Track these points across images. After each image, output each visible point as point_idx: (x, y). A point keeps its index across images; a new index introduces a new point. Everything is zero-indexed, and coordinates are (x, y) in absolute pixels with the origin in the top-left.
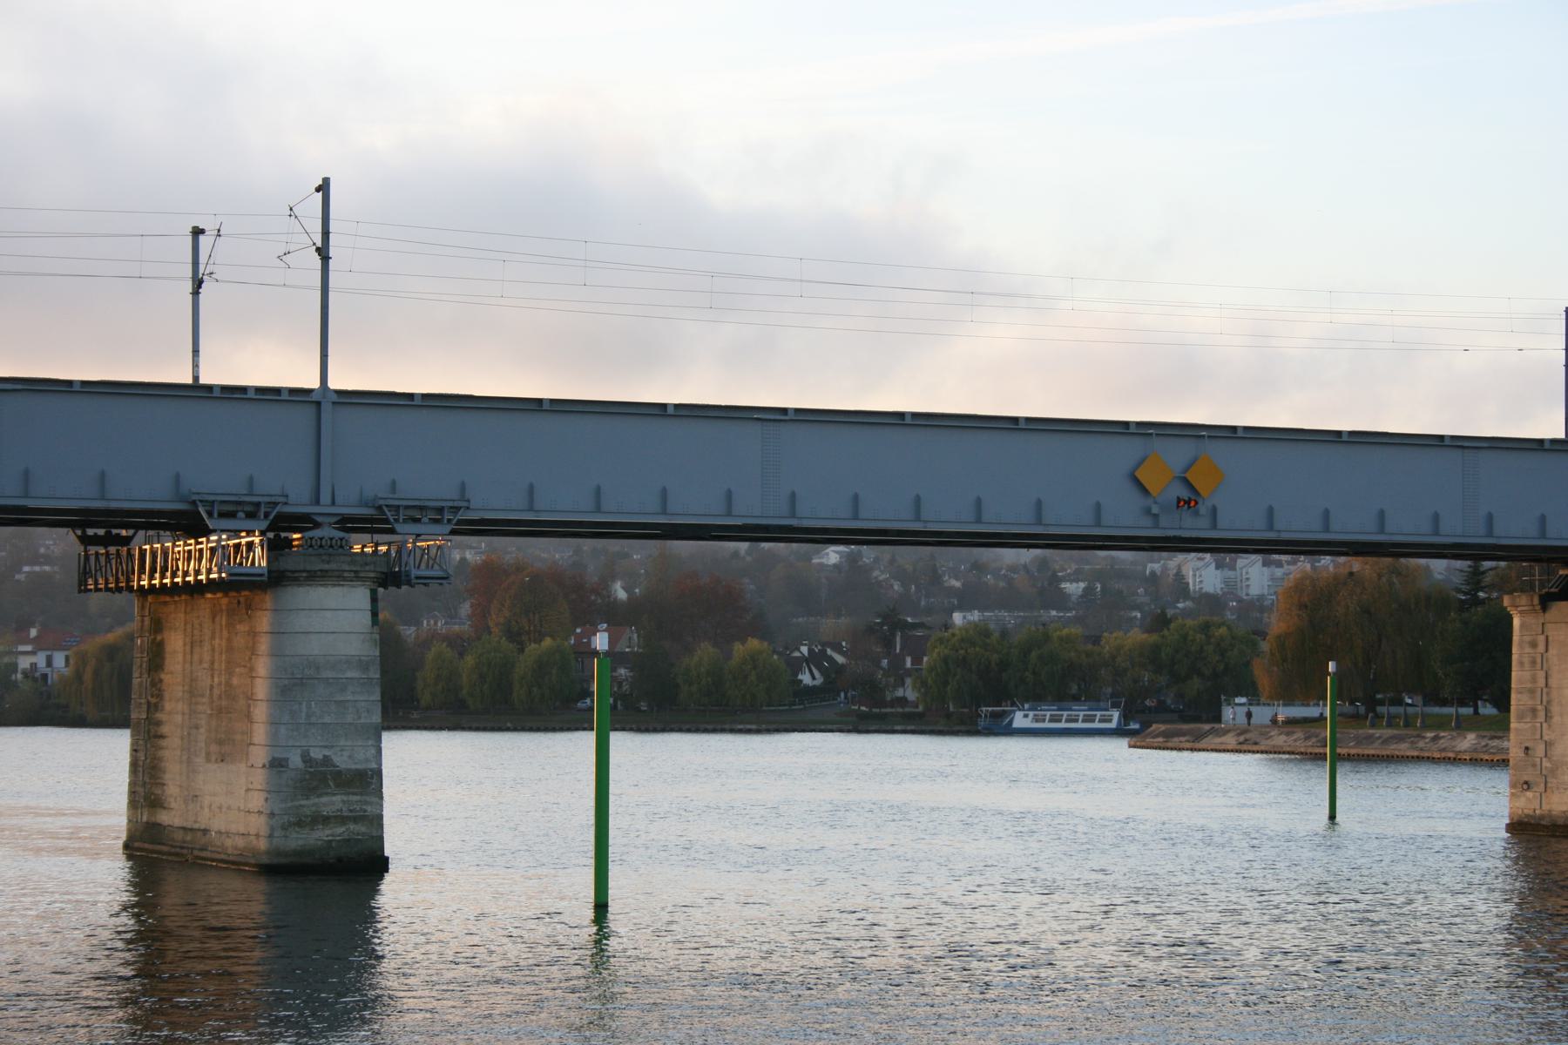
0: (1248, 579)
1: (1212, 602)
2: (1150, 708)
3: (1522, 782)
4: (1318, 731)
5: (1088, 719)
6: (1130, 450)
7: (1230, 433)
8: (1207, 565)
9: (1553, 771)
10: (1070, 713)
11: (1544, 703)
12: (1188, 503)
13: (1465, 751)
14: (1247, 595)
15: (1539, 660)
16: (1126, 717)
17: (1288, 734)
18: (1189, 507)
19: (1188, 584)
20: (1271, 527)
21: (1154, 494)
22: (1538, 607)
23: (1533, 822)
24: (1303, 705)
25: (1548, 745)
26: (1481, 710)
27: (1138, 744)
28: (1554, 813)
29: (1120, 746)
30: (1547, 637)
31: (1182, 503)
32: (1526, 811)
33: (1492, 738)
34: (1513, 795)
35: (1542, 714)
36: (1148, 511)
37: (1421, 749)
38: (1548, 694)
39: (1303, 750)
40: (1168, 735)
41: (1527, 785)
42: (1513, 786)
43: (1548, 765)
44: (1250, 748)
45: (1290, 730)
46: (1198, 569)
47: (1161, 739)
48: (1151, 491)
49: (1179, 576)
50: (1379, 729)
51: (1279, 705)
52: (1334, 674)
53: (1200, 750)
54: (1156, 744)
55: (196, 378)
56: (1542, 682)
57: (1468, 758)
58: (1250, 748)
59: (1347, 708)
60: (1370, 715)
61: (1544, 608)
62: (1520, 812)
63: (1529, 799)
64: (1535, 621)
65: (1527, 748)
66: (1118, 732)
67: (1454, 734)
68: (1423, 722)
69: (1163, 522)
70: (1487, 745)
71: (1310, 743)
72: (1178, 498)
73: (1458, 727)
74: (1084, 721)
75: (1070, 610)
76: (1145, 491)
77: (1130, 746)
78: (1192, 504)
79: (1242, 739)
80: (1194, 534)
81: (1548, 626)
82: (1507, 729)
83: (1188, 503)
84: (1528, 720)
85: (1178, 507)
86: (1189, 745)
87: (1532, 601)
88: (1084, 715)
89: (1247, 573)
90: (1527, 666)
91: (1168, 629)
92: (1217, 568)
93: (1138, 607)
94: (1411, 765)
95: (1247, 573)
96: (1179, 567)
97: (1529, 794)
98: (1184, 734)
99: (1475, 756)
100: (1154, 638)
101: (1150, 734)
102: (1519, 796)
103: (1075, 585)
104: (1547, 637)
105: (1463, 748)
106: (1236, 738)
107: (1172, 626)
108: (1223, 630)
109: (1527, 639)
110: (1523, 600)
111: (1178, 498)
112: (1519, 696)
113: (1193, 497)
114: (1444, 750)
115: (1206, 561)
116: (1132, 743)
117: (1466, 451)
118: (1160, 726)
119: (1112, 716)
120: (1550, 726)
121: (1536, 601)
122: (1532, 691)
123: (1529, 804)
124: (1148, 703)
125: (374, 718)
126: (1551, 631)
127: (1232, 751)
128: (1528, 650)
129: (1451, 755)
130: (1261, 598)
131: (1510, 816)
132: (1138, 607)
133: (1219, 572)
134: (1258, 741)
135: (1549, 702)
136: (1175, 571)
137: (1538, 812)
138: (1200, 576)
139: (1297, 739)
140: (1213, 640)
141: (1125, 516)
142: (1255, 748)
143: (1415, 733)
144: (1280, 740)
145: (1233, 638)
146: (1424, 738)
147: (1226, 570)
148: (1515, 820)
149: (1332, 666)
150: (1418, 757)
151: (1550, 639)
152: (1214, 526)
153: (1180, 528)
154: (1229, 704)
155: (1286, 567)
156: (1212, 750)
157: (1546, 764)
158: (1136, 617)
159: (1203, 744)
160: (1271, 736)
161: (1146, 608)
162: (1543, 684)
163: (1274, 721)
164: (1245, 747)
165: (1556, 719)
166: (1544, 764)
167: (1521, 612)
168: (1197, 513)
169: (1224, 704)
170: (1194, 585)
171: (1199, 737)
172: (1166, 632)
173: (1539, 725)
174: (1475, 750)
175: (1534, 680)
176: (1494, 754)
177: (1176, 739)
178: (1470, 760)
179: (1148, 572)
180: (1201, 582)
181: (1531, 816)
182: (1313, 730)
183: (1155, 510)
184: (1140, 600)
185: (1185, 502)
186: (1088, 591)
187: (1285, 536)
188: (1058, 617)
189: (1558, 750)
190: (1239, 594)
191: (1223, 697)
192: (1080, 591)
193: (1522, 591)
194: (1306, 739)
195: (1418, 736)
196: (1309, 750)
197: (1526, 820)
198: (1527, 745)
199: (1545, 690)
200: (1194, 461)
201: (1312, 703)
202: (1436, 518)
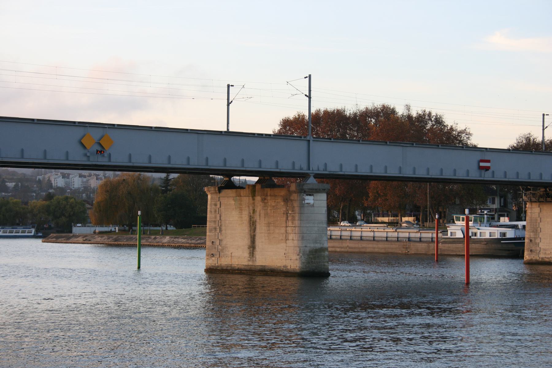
0: (74, 182)
1: (62, 190)
2: (46, 228)
3: (211, 254)
4: (112, 236)
5: (23, 232)
6: (80, 132)
7: (112, 126)
8: (59, 177)
9: (222, 250)
10: (4, 230)
11: (219, 226)
12: (101, 152)
13: (166, 243)
14: (74, 187)
15: (217, 210)
16: (37, 231)
17: (101, 237)
18: (101, 154)
19: (52, 183)
20: (130, 161)
21: (88, 149)
22: (218, 192)
23: (214, 268)
24: (101, 227)
25: (220, 241)
26: (169, 228)
27: (46, 241)
28: (222, 265)
29: (39, 241)
30: (220, 202)
31: (99, 152)
32: (212, 265)
33: (175, 238)
34: (207, 259)
35: (218, 230)
36: (85, 155)
37: (150, 242)
38: (220, 222)
39: (107, 243)
40: (57, 238)
41: (213, 255)
42: (207, 255)
43: (220, 248)
44: (88, 242)
45: (102, 235)
46: (56, 178)
47: (54, 239)
48: (87, 147)
49: (49, 181)
50: (134, 235)
51: (96, 227)
52: (140, 215)
53: (69, 243)
54: (53, 241)
55: (228, 129)
56: (218, 218)
57: (167, 245)
58: (88, 242)
59: (122, 228)
60: (131, 230)
61: (220, 192)
62: (210, 265)
63: (213, 260)
64: (216, 196)
65: (213, 242)
66: (35, 237)
67: (162, 237)
68: (150, 232)
69: (91, 159)
70: (173, 240)
71: (110, 240)
72: (97, 150)
73: (162, 234)
74: (22, 233)
75: (10, 192)
76: (85, 147)
77: (42, 242)
78: (102, 152)
79: (84, 239)
80: (103, 164)
81: (221, 198)
82: (206, 235)
83: (101, 152)
84: (213, 232)
85: (97, 153)
86: (65, 241)
87: (215, 189)
88: (9, 231)
89: (73, 180)
90: (213, 213)
91: (54, 199)
92: (63, 178)
93: (34, 192)
94: (147, 248)
95: (73, 180)
96: (49, 177)
97: (213, 258)
98: (63, 237)
99: (169, 244)
100: (47, 203)
101: (50, 237)
102: (210, 259)
103: (11, 184)
104: (220, 202)
105: (165, 242)
106: (82, 239)
107: (55, 198)
108: (72, 200)
109: (213, 203)
110: (212, 189)
111: (97, 150)
112: (210, 223)
113: (102, 150)
114: (158, 242)
115: (59, 175)
116: (44, 241)
117: (199, 135)
118: (54, 234)
119: (32, 231)
120: (221, 234)
121: (217, 189)
122: (215, 222)
123: (213, 262)
124: (45, 226)
125: (527, 256)
126: (222, 200)
127: (81, 243)
128: (213, 207)
129: (161, 244)
130: (79, 188)
131: (206, 266)
132: (34, 192)
133: (63, 179)
134: (91, 239)
135: (221, 225)
136: (47, 179)
137: (216, 265)
138: (57, 181)
139: (105, 239)
140: (69, 203)
141: (77, 157)
142: (90, 242)
143: (147, 236)
144: (99, 239)
145: (76, 203)
146: (151, 238)
147: (66, 179)
148: (208, 267)
149: (139, 213)
150: (149, 245)
151: (222, 203)
152: (110, 161)
153: (98, 161)
154: (75, 227)
155: (87, 178)
156: (74, 243)
157: (220, 247)
158: (34, 195)
159: (70, 241)
160: (95, 238)
161: (37, 192)
162: (219, 219)
163: (95, 232)
164: (86, 242)
165: (223, 232)
166: (219, 247)
167: (211, 193)
168: (103, 156)
169: (73, 226)
170: (54, 183)
171: (69, 238)
172: (52, 201)
173: (217, 234)
174: (169, 242)
175: (216, 217)
176: (176, 243)
177: (60, 239)
178: (168, 246)
179: (37, 179)
180: (57, 183)
181: (214, 266)
182: (110, 236)
183: (88, 155)
184: (35, 189)
185: (100, 152)
186: (16, 186)
187: (135, 165)
188: (5, 195)
189: (224, 243)
190: (70, 187)
191: (73, 224)
192: (13, 186)
193: (212, 185)
194: (108, 239)
195: (149, 237)
196: (109, 243)
197: (212, 268)
198: (213, 241)
199: (219, 221)
200: (102, 137)
201: (104, 226)
202: (188, 159)
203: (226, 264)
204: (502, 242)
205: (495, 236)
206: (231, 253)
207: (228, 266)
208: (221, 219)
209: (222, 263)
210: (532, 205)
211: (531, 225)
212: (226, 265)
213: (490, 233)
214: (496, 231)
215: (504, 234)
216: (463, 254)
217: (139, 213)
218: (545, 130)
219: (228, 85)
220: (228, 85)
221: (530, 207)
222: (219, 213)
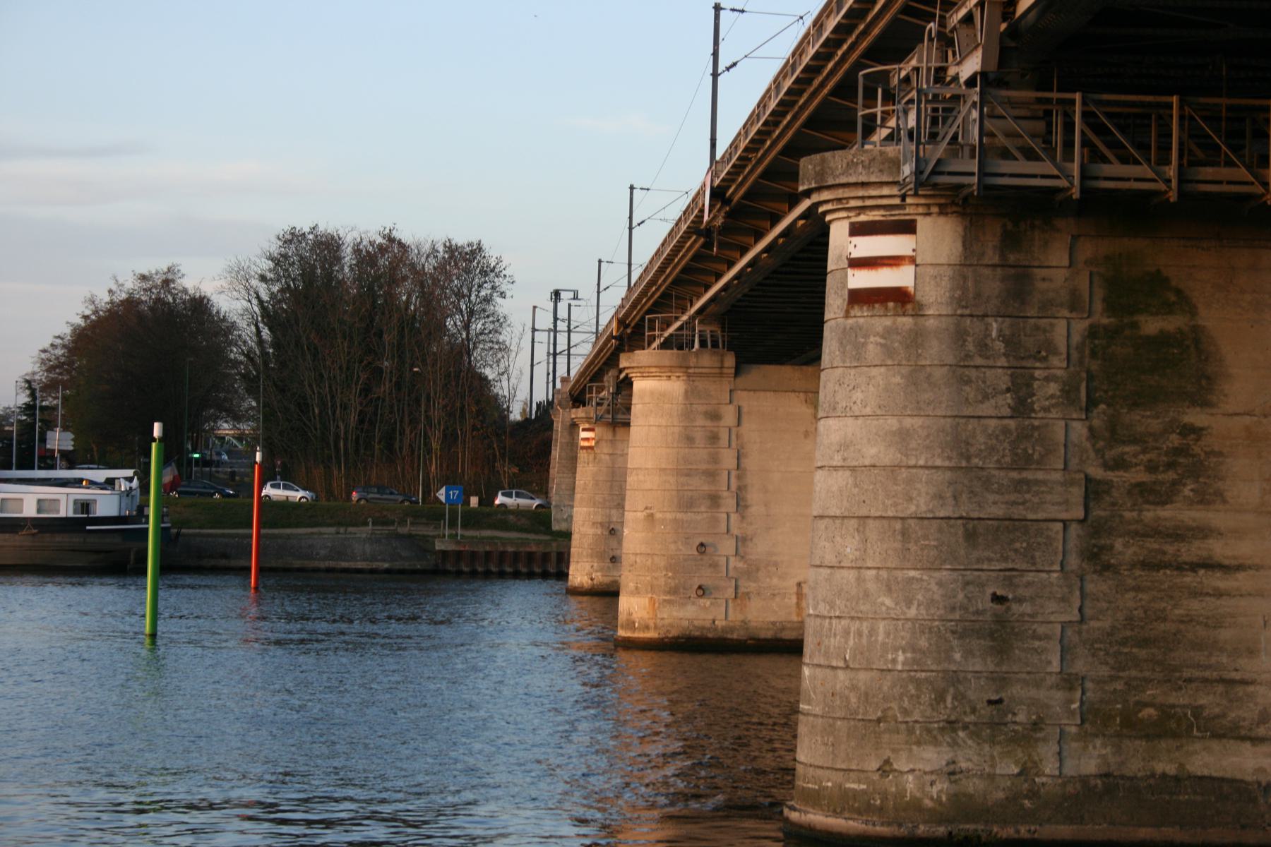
9: (752, 572)
25: (742, 541)
28: (753, 624)
35: (729, 503)
43: (740, 565)
62: (686, 623)
135: (741, 489)
149: (157, 429)
151: (745, 410)
181: (709, 629)
189: (759, 549)
199: (734, 473)
203: (772, 619)
204: (88, 528)
205: (58, 512)
207: (783, 629)
209: (750, 617)
211: (611, 487)
212: (774, 623)
213: (39, 501)
214: (63, 499)
215: (85, 506)
216: (242, 563)
217: (157, 429)
222: (734, 444)
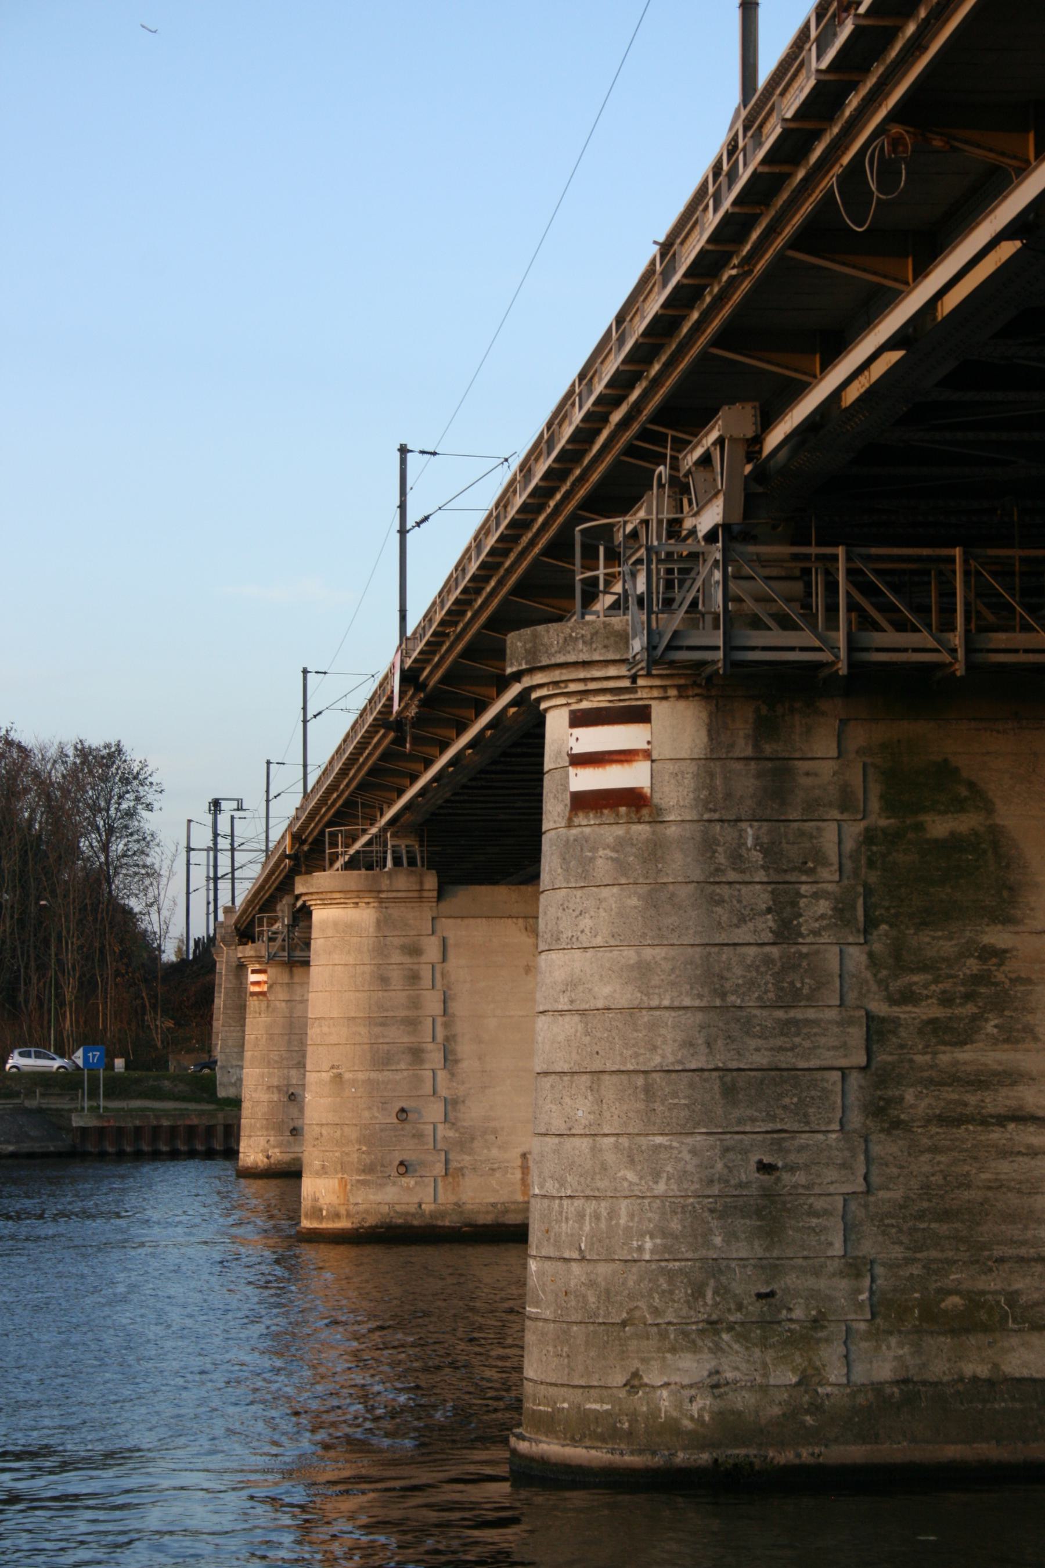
9: (465, 1142)
25: (452, 1104)
35: (435, 1057)
43: (451, 1134)
62: (385, 1209)
84: (403, 1066)
87: (421, 883)
151: (451, 942)
165: (467, 1065)
175: (415, 1003)
181: (413, 1215)
189: (473, 1113)
197: (400, 1221)
199: (439, 1021)
203: (492, 1200)
206: (524, 1156)
207: (506, 1211)
208: (450, 1011)
210: (291, 971)
211: (289, 1042)
212: (494, 1205)
218: (309, 724)
219: (401, 445)
220: (401, 445)
221: (286, 980)
222: (439, 986)
